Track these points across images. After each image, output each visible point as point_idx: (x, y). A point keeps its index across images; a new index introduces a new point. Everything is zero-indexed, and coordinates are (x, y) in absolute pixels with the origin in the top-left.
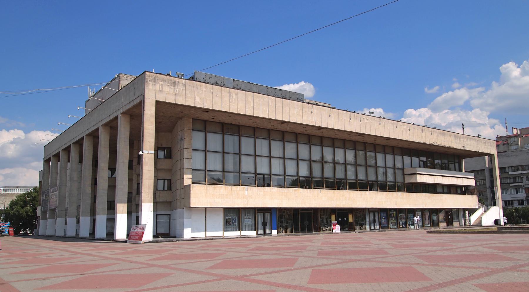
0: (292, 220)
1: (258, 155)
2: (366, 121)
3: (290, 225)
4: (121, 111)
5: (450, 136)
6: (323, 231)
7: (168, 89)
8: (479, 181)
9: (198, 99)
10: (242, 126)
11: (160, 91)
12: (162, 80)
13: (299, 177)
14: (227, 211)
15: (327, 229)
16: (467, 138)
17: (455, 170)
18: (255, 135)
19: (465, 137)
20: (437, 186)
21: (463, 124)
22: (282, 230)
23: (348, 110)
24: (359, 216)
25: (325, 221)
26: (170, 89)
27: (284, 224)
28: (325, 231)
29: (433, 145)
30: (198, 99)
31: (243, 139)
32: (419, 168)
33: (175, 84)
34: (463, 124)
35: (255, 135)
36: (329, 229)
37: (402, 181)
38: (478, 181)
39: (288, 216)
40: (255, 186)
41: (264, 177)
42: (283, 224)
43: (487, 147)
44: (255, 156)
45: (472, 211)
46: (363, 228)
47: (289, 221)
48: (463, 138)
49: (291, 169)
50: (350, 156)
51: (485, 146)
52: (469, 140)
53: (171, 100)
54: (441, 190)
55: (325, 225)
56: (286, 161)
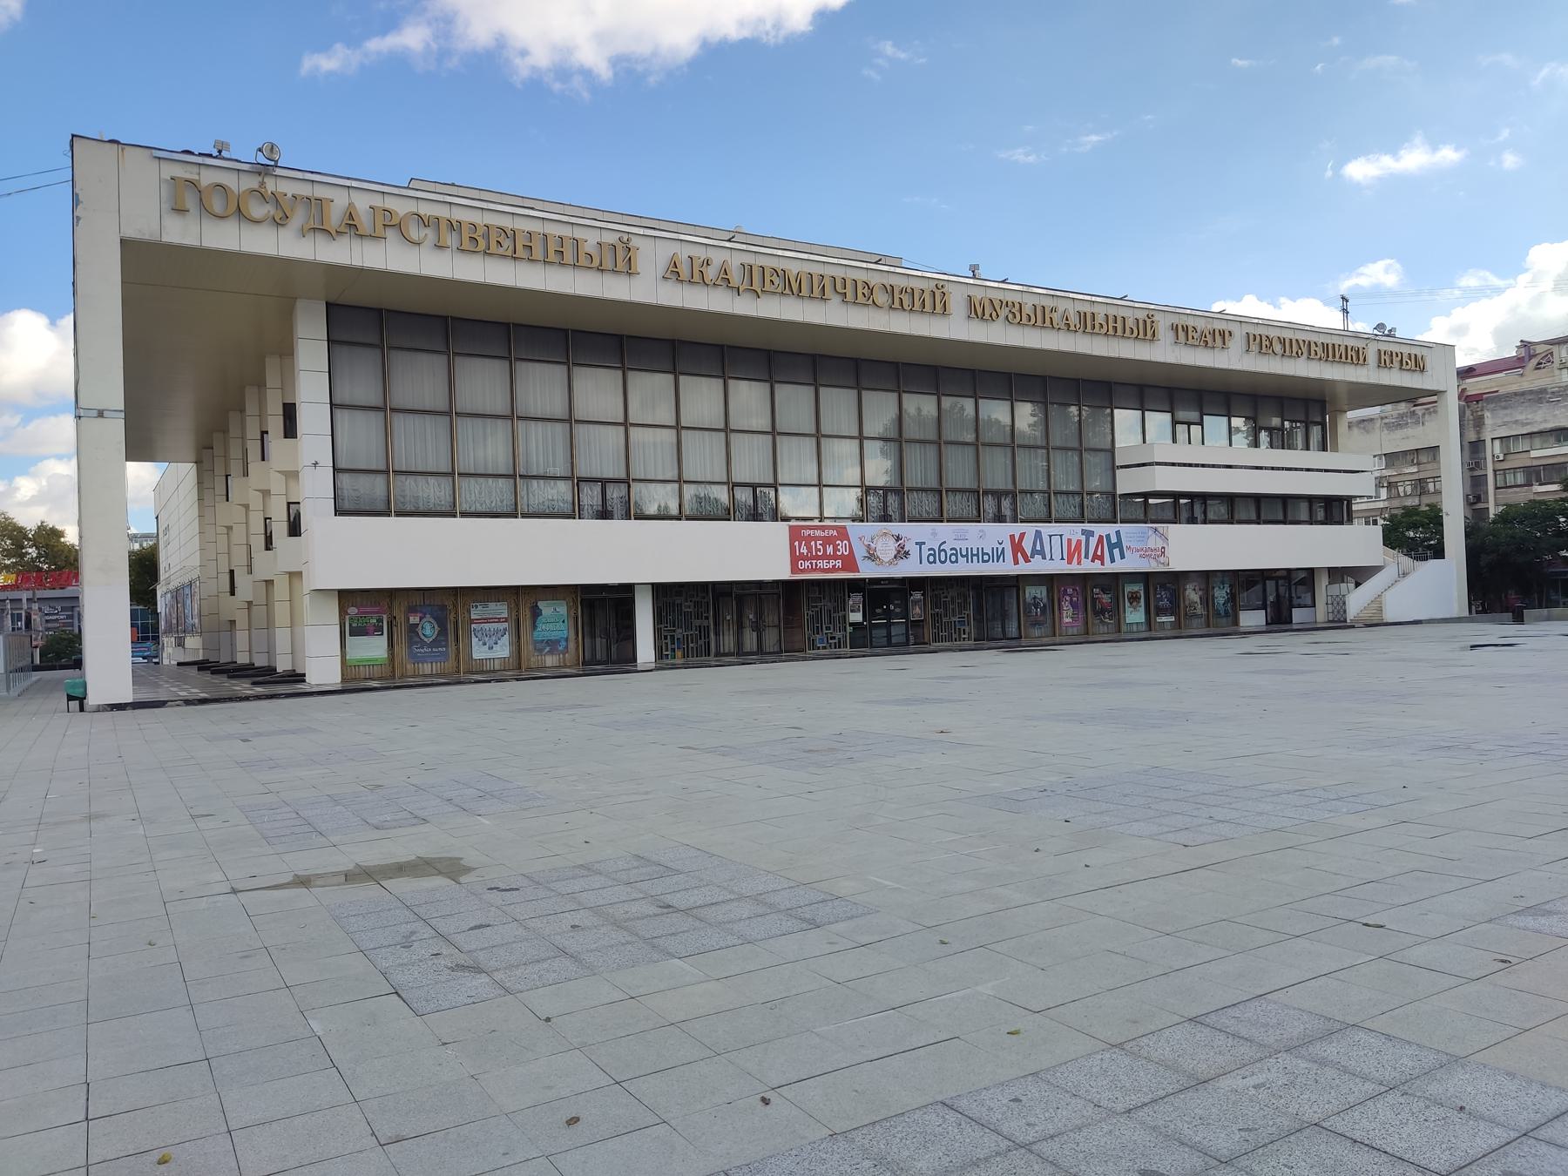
0: (707, 618)
1: (735, 428)
3: (700, 632)
6: (819, 648)
8: (1434, 482)
10: (682, 342)
13: (733, 486)
15: (830, 641)
17: (1283, 448)
18: (815, 380)
20: (1237, 499)
21: (1343, 298)
22: (673, 650)
23: (1125, 297)
24: (949, 599)
25: (825, 618)
27: (680, 631)
28: (824, 648)
29: (1293, 376)
31: (783, 391)
32: (1306, 452)
34: (1343, 298)
35: (815, 380)
36: (839, 642)
37: (1110, 489)
38: (1432, 480)
39: (692, 607)
40: (729, 520)
41: (1146, 502)
42: (674, 631)
44: (818, 436)
45: (1359, 575)
46: (960, 635)
47: (697, 623)
49: (703, 458)
50: (1026, 416)
54: (1304, 516)
55: (825, 631)
56: (778, 438)
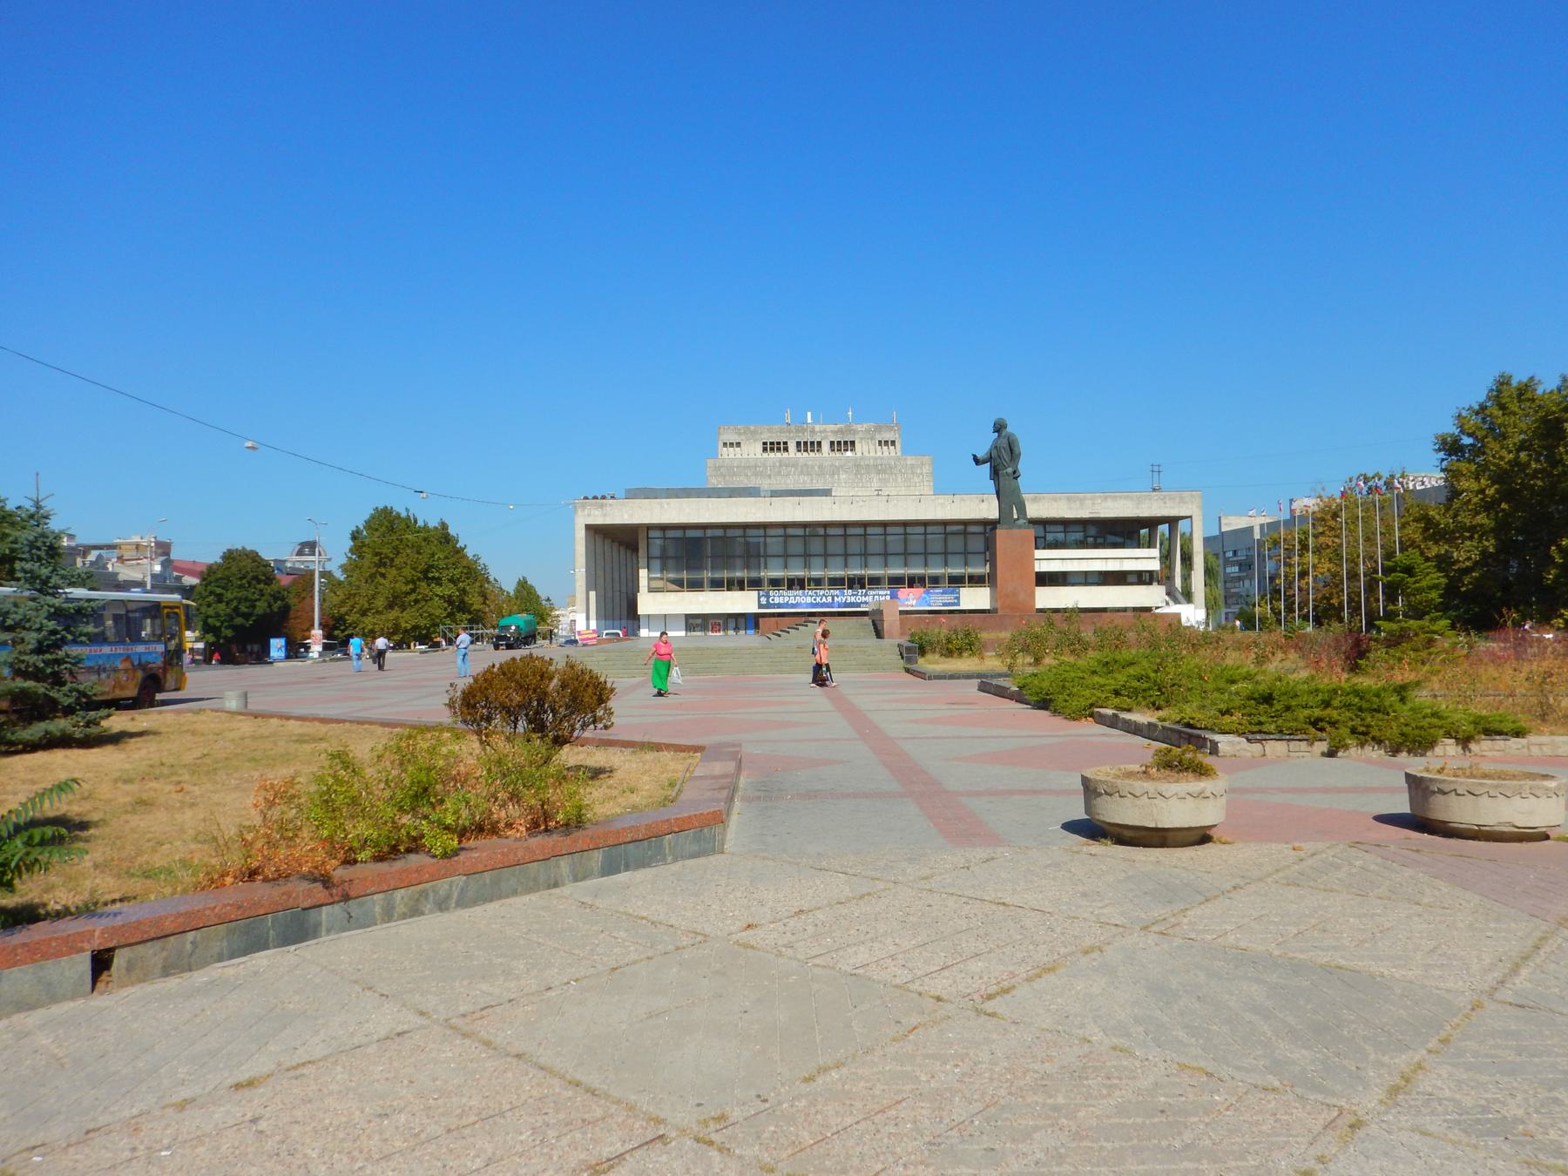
2: (862, 503)
5: (1055, 500)
7: (596, 512)
9: (626, 516)
11: (589, 515)
12: (591, 505)
14: (688, 617)
16: (1106, 498)
19: (1100, 497)
26: (597, 512)
30: (626, 516)
33: (602, 506)
43: (1168, 505)
48: (1092, 499)
51: (1163, 505)
52: (1109, 500)
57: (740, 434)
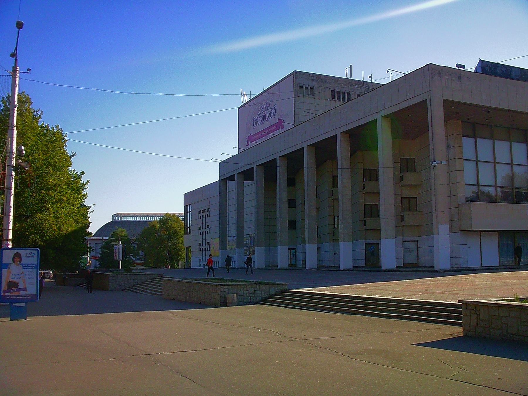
4: (383, 113)
53: (457, 98)
57: (313, 80)
